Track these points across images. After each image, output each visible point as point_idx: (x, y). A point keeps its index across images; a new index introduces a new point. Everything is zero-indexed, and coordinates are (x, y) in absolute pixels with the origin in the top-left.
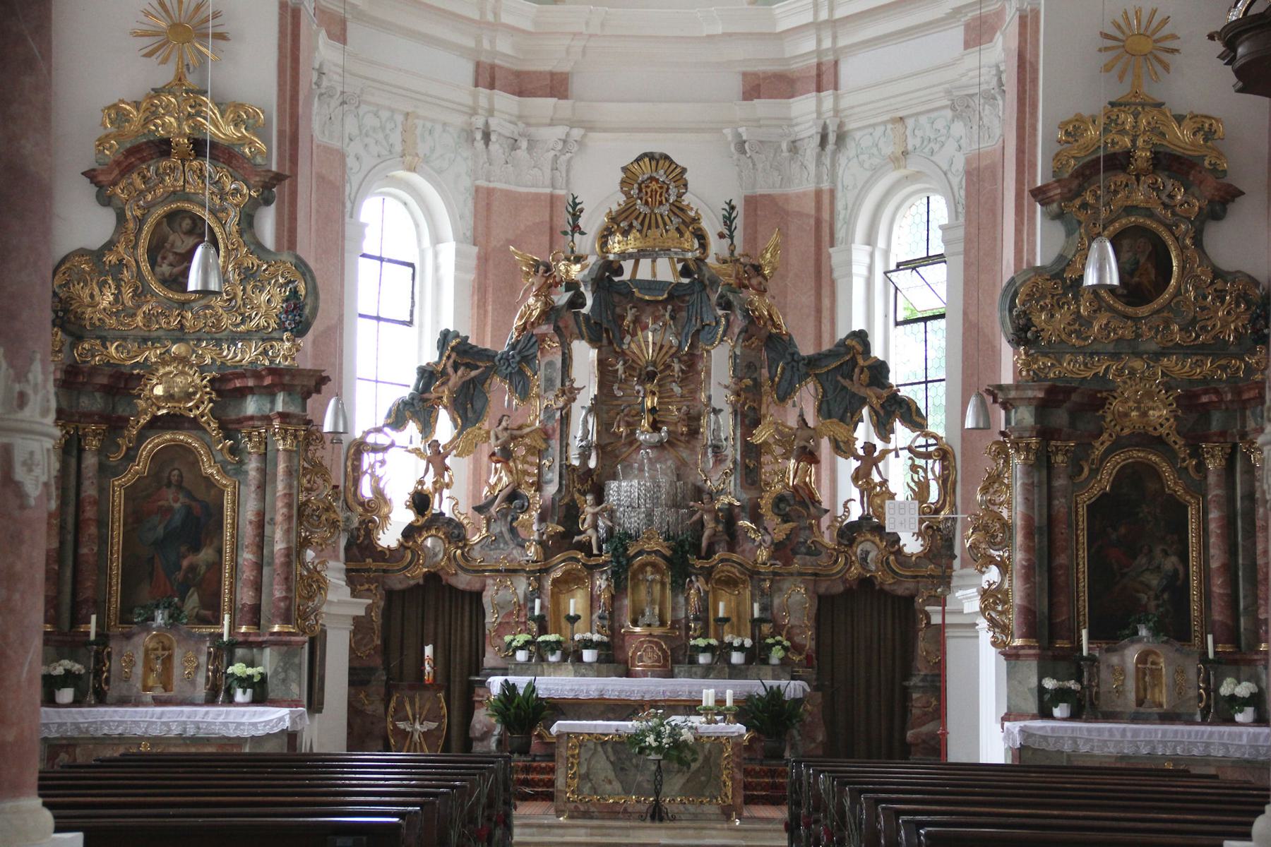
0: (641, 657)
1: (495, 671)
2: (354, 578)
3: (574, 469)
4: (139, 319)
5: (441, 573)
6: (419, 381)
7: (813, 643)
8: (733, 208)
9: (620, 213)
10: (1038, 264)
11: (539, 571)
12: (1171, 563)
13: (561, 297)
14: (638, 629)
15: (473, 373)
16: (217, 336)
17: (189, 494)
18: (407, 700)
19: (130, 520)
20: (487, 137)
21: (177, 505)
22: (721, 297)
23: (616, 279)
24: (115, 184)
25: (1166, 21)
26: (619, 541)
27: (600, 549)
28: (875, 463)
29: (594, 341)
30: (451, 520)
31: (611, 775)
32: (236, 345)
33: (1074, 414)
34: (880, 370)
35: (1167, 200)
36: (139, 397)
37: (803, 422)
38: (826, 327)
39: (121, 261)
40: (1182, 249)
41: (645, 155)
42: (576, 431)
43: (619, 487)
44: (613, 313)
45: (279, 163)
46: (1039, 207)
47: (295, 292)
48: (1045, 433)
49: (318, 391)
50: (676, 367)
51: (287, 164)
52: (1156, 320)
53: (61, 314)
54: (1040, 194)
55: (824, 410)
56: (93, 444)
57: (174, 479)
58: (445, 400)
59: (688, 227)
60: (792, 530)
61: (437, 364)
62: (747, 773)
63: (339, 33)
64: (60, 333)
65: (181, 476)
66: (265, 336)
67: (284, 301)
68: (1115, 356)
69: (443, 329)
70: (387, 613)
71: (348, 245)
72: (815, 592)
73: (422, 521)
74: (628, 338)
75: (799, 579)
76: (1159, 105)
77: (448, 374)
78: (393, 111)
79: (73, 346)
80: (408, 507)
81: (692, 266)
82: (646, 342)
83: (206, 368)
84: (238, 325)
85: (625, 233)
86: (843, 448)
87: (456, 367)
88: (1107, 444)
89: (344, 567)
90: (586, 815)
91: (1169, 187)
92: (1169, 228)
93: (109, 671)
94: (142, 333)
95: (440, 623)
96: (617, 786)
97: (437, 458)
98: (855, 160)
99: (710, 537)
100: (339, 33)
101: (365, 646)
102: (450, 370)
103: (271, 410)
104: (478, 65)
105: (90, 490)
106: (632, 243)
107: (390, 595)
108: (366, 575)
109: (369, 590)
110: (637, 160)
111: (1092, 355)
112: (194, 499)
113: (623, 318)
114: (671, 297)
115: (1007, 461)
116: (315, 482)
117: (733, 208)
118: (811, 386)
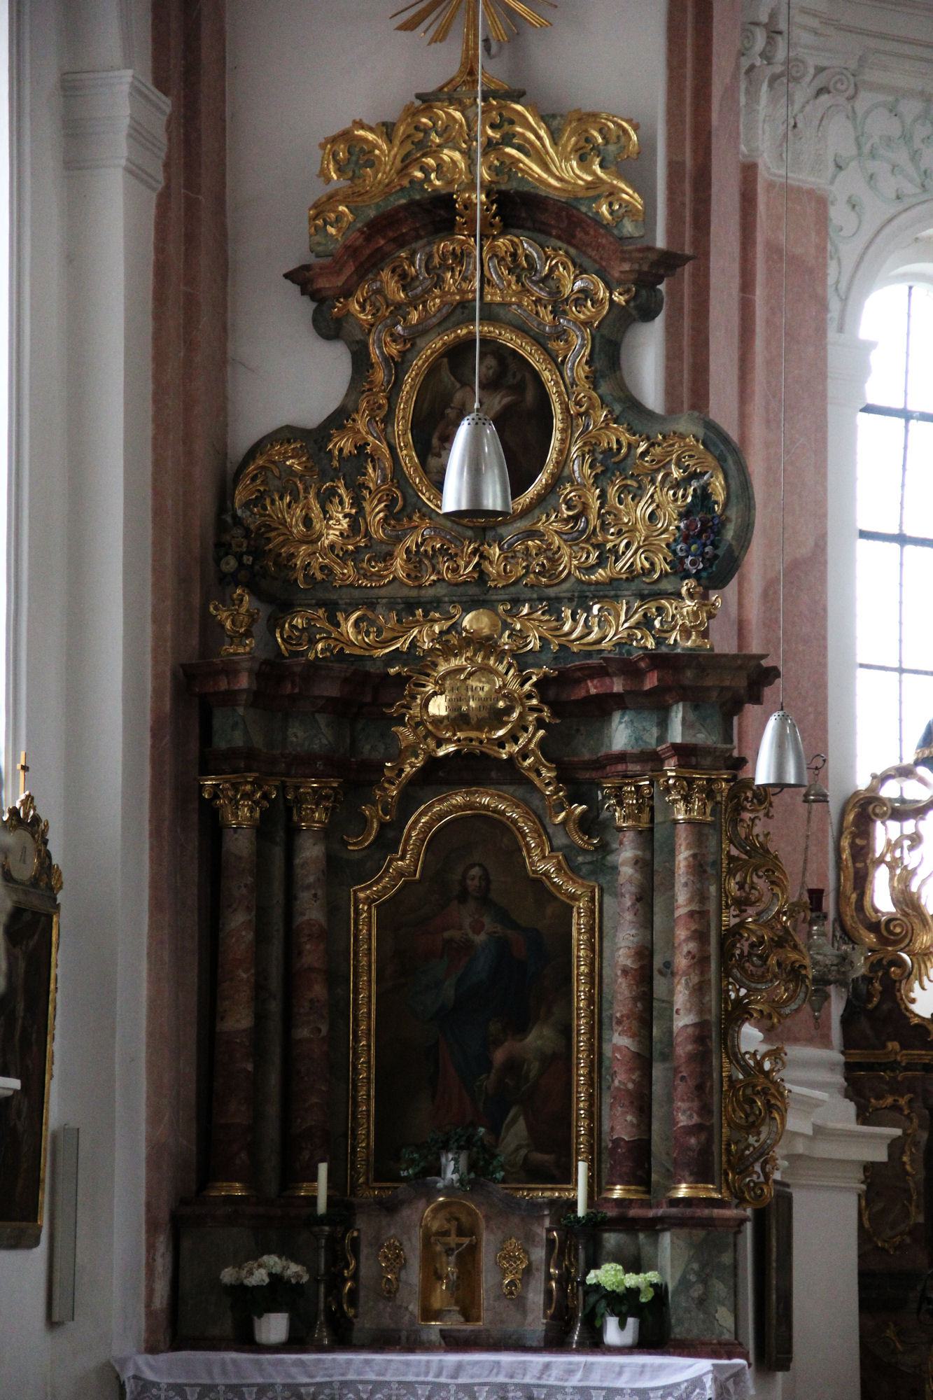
16: (552, 592)
17: (503, 916)
21: (480, 938)
24: (348, 293)
32: (588, 610)
36: (400, 721)
45: (671, 233)
47: (704, 497)
57: (472, 884)
65: (486, 877)
67: (681, 516)
83: (530, 659)
84: (591, 569)
89: (841, 1058)
93: (355, 1277)
94: (405, 592)
103: (661, 739)
105: (311, 911)
108: (886, 1075)
109: (895, 1107)
116: (753, 887)
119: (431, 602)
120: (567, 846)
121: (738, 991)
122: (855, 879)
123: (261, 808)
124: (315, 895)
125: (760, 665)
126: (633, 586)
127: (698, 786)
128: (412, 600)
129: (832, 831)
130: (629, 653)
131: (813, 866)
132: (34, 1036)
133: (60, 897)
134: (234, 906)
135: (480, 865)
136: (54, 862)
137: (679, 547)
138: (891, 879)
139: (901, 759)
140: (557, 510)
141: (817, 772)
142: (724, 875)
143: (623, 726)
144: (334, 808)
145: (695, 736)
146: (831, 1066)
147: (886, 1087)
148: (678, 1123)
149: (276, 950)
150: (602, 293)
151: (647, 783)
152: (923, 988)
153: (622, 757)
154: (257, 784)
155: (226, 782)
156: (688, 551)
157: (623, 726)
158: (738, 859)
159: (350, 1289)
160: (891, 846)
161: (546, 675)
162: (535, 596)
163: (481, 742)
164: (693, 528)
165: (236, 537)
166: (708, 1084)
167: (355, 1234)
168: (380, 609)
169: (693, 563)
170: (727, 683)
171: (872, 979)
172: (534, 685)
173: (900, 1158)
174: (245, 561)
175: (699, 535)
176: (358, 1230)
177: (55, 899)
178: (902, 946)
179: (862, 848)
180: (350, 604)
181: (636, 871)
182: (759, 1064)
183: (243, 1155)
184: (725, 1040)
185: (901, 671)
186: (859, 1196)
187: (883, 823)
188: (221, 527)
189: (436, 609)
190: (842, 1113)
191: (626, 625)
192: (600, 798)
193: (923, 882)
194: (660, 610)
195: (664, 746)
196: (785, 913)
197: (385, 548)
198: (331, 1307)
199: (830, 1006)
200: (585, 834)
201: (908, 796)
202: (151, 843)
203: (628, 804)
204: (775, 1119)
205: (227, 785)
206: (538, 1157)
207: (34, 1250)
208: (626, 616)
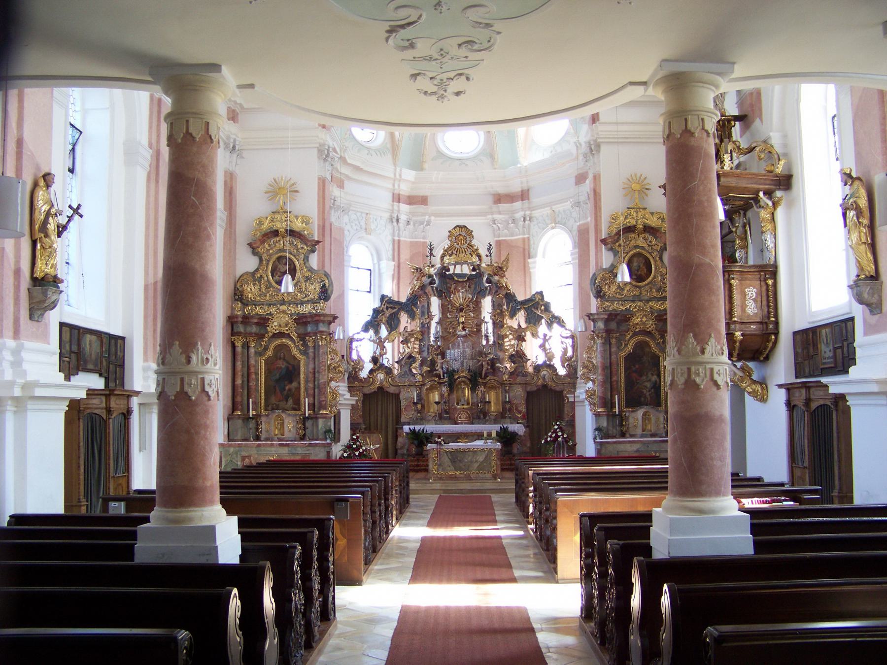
0: (460, 418)
1: (405, 424)
2: (351, 389)
3: (433, 346)
6: (373, 314)
7: (525, 410)
8: (491, 245)
9: (448, 248)
10: (604, 267)
11: (421, 385)
12: (654, 378)
13: (426, 280)
14: (458, 407)
15: (394, 311)
17: (288, 362)
20: (398, 220)
21: (283, 366)
22: (487, 279)
23: (447, 273)
24: (258, 247)
25: (645, 178)
26: (451, 373)
27: (444, 376)
28: (547, 340)
29: (440, 297)
31: (450, 464)
33: (619, 324)
34: (547, 307)
35: (649, 244)
37: (519, 326)
38: (528, 289)
39: (261, 276)
40: (655, 261)
41: (457, 226)
42: (433, 331)
43: (450, 352)
44: (446, 286)
45: (318, 237)
46: (603, 246)
47: (324, 286)
48: (608, 331)
49: (334, 322)
50: (471, 306)
51: (321, 236)
52: (647, 288)
54: (604, 241)
55: (528, 320)
56: (253, 344)
57: (282, 356)
58: (383, 321)
59: (474, 252)
60: (516, 367)
61: (380, 307)
62: (501, 460)
63: (341, 186)
65: (284, 355)
66: (313, 302)
68: (633, 301)
71: (346, 263)
72: (526, 391)
73: (376, 367)
74: (452, 295)
75: (520, 386)
76: (645, 209)
78: (362, 213)
81: (476, 267)
82: (460, 297)
84: (303, 298)
85: (450, 256)
86: (535, 335)
87: (387, 308)
88: (631, 334)
90: (441, 479)
91: (650, 239)
92: (650, 253)
96: (452, 468)
97: (380, 343)
98: (537, 226)
99: (486, 371)
100: (341, 186)
102: (385, 310)
103: (317, 330)
104: (393, 194)
105: (252, 362)
106: (453, 259)
107: (365, 395)
110: (454, 228)
111: (624, 301)
112: (290, 364)
113: (450, 288)
114: (469, 279)
115: (594, 342)
117: (491, 245)
129: (345, 344)
146: (345, 387)
150: (306, 248)
165: (238, 293)
190: (348, 395)
206: (294, 406)
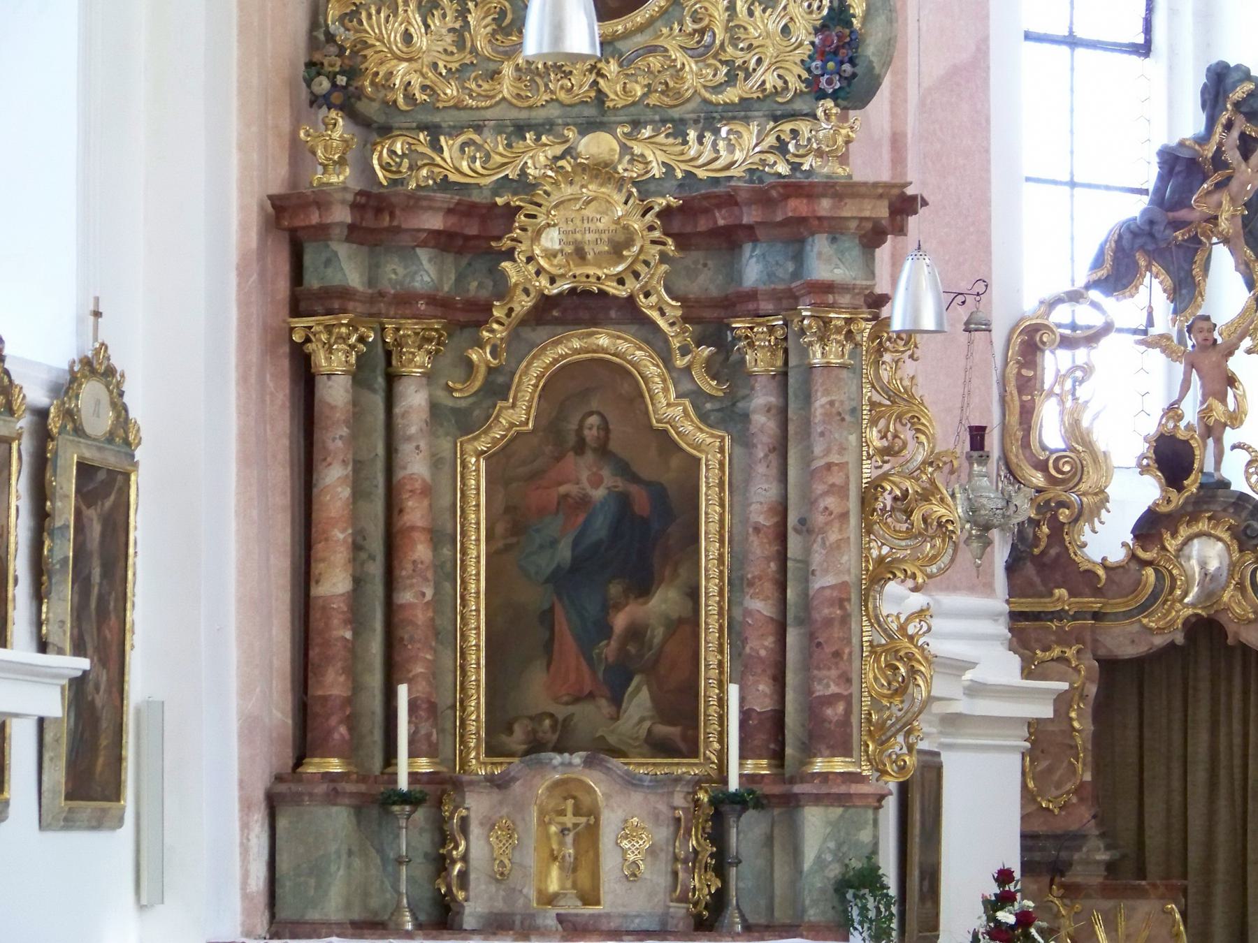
4: (506, 88)
5: (1223, 619)
16: (676, 113)
17: (624, 469)
18: (1098, 917)
19: (500, 528)
21: (599, 494)
30: (1243, 497)
32: (716, 132)
36: (509, 255)
53: (342, 80)
56: (417, 362)
57: (591, 434)
58: (1224, 225)
61: (1203, 140)
64: (340, 121)
65: (605, 427)
67: (817, 31)
69: (1214, 61)
70: (1102, 710)
73: (1177, 499)
77: (1226, 165)
79: (368, 147)
80: (1144, 470)
83: (652, 187)
84: (717, 89)
89: (1006, 608)
93: (465, 858)
94: (514, 114)
95: (1223, 730)
101: (1058, 785)
102: (1232, 156)
103: (796, 275)
107: (1110, 668)
108: (1054, 625)
109: (1062, 659)
112: (635, 478)
116: (896, 436)
118: (1029, 564)
119: (543, 125)
120: (694, 392)
121: (880, 548)
122: (1021, 413)
123: (357, 352)
124: (418, 447)
125: (903, 193)
126: (766, 106)
127: (835, 326)
128: (522, 123)
130: (761, 181)
131: (975, 400)
132: (112, 604)
133: (139, 454)
134: (329, 459)
135: (599, 413)
136: (131, 416)
137: (814, 64)
138: (1062, 413)
139: (1073, 281)
140: (681, 24)
141: (978, 298)
142: (865, 422)
143: (754, 260)
144: (437, 351)
145: (832, 271)
146: (994, 616)
147: (1053, 638)
148: (813, 693)
149: (377, 506)
151: (781, 322)
152: (1094, 531)
153: (752, 295)
154: (353, 326)
155: (318, 324)
156: (824, 67)
157: (754, 260)
158: (880, 405)
159: (460, 871)
160: (1060, 378)
161: (668, 206)
162: (657, 118)
163: (599, 278)
164: (828, 44)
166: (847, 651)
167: (464, 812)
168: (486, 132)
169: (829, 82)
170: (867, 214)
171: (1039, 521)
172: (659, 215)
173: (1068, 713)
174: (338, 83)
175: (835, 53)
176: (467, 809)
177: (133, 456)
178: (1071, 485)
179: (1029, 379)
180: (454, 127)
181: (769, 419)
182: (903, 628)
183: (343, 730)
184: (866, 601)
185: (1073, 184)
186: (1023, 755)
187: (1053, 352)
188: (313, 44)
189: (549, 132)
191: (757, 149)
192: (730, 339)
193: (1096, 417)
194: (795, 133)
195: (799, 283)
196: (931, 464)
197: (492, 66)
198: (439, 890)
199: (993, 552)
200: (713, 378)
201: (1080, 321)
202: (238, 393)
203: (759, 346)
204: (919, 686)
205: (321, 328)
206: (663, 730)
207: (119, 831)
208: (757, 139)
